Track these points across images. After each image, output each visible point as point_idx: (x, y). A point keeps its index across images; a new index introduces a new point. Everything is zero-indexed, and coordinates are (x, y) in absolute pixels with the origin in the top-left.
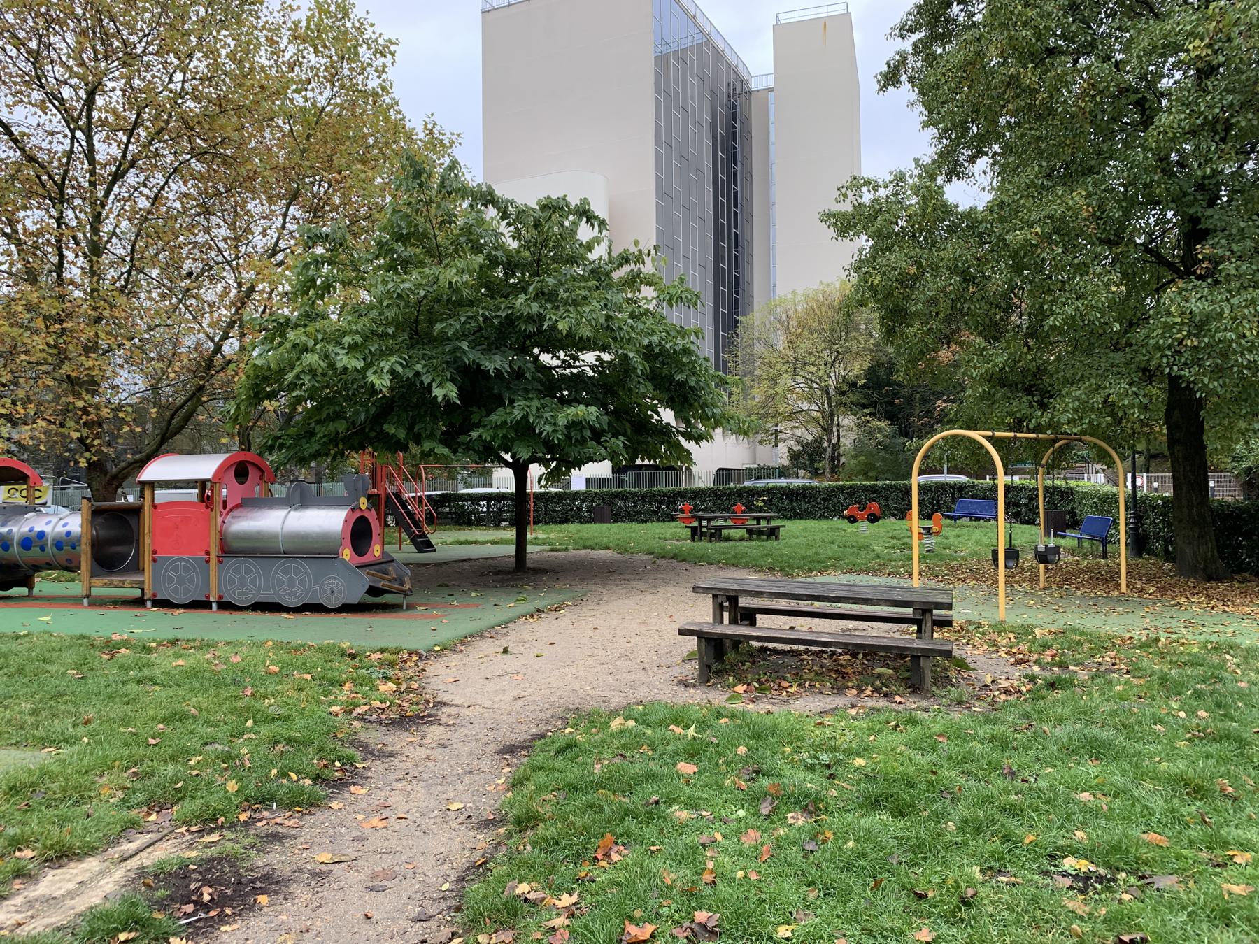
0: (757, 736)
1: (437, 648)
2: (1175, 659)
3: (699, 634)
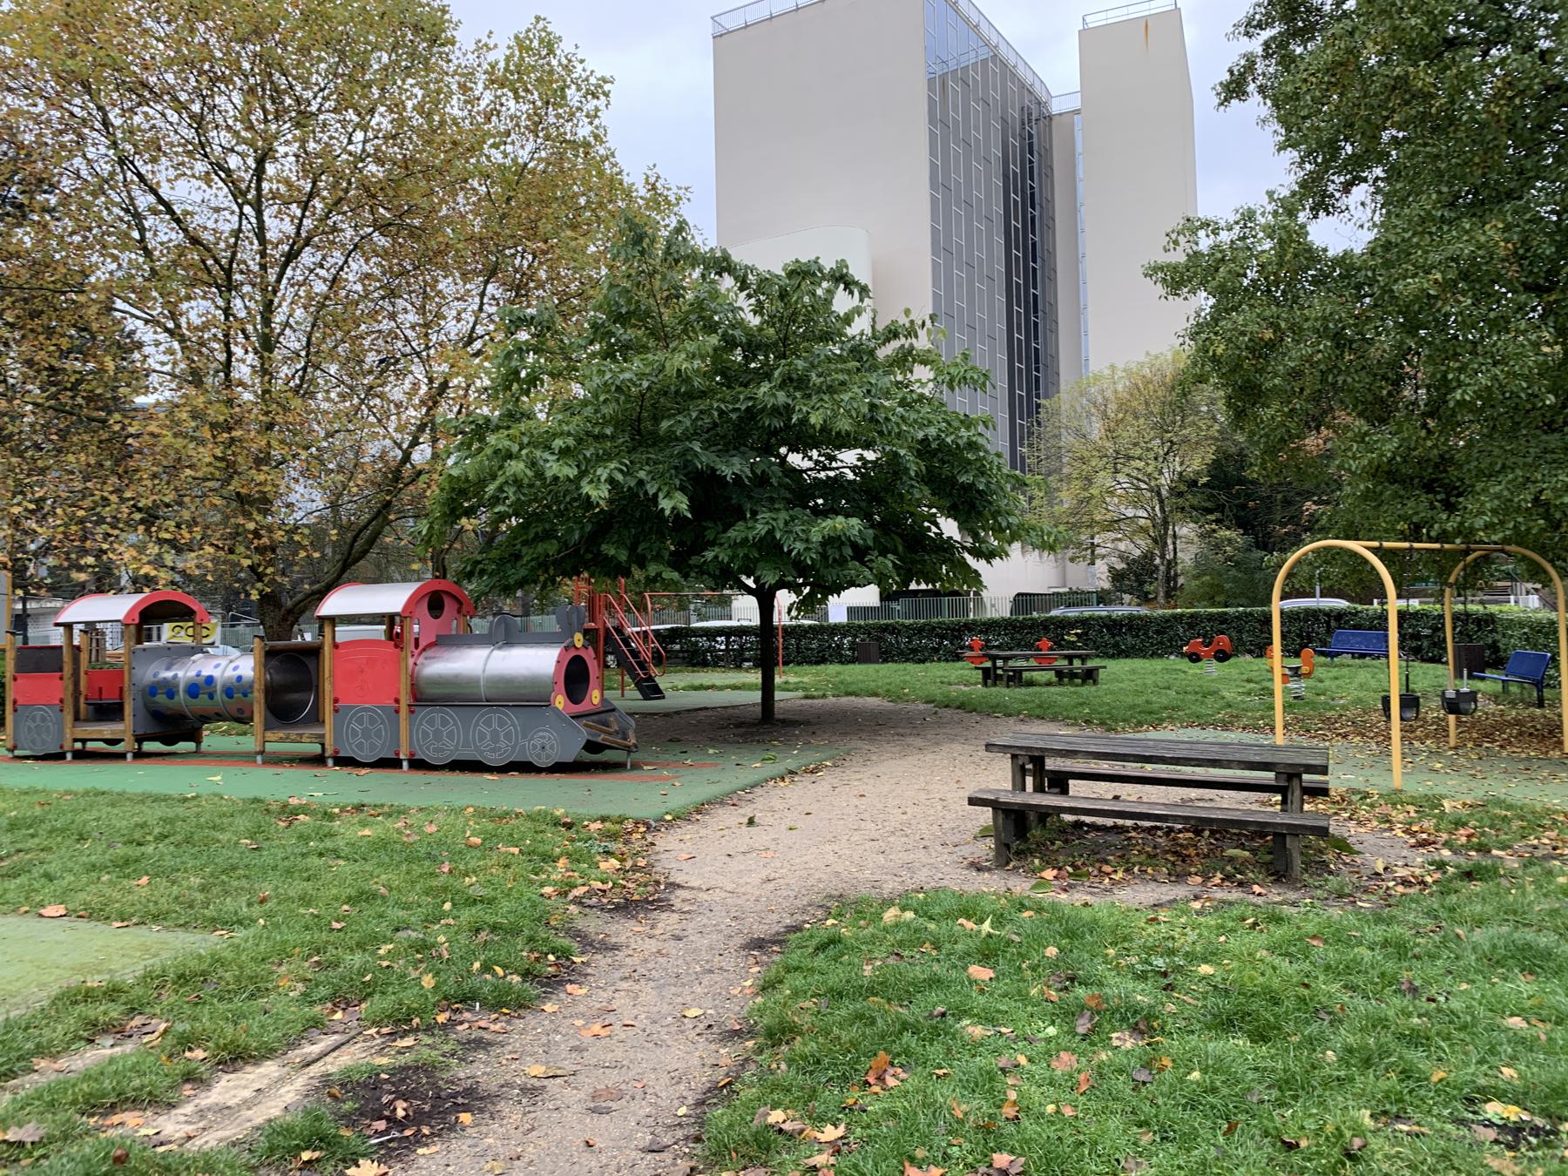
0: (1071, 934)
1: (668, 817)
3: (995, 805)
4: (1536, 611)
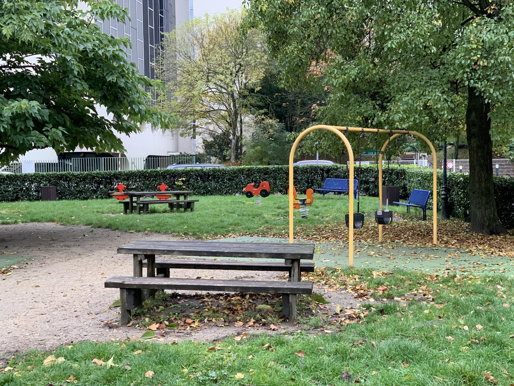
0: (162, 362)
2: (464, 289)
3: (122, 286)
4: (426, 168)
